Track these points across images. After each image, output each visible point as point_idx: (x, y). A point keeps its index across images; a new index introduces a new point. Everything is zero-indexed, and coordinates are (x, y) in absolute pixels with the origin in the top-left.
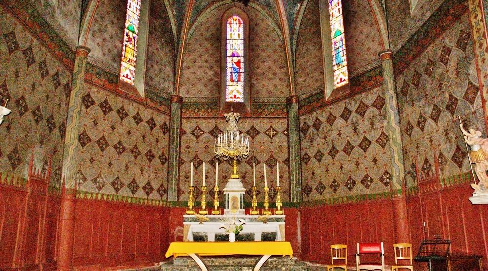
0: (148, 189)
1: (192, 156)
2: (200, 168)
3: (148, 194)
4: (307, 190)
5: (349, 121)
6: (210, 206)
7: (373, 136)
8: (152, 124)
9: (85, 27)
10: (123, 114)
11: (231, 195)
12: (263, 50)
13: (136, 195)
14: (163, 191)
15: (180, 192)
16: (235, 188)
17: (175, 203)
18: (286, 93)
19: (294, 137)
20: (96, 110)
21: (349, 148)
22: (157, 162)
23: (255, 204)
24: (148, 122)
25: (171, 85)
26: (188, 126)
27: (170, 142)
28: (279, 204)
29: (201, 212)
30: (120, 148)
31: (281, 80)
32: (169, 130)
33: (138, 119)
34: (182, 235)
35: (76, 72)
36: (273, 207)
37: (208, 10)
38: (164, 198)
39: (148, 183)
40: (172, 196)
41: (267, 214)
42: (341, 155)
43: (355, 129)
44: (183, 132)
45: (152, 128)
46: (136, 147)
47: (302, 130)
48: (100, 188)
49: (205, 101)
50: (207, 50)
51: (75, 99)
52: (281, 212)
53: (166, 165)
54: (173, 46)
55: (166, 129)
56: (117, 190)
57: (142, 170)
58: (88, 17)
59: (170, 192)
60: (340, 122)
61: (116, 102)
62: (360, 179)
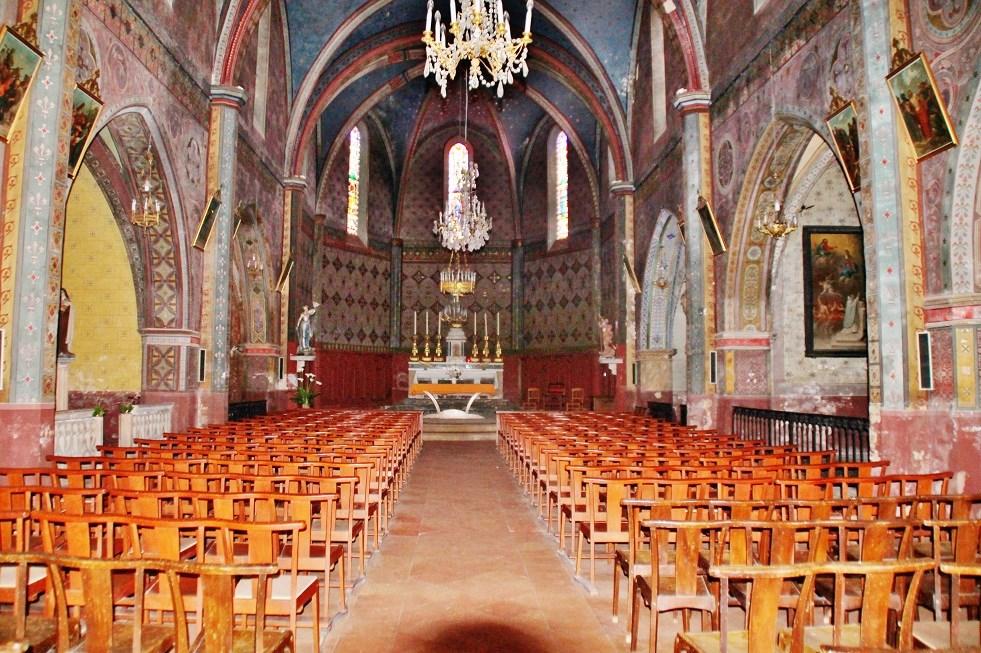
0: (374, 336)
1: (413, 301)
2: (423, 313)
3: (373, 341)
4: (527, 338)
5: (566, 276)
6: (433, 354)
7: (583, 294)
8: (375, 272)
9: (320, 195)
10: (351, 268)
11: (453, 343)
12: (488, 187)
13: (364, 343)
14: (386, 337)
15: (402, 339)
16: (456, 337)
17: (396, 349)
18: (511, 236)
19: (517, 282)
20: (331, 268)
21: (564, 302)
22: (380, 309)
23: (476, 352)
24: (372, 272)
25: (391, 228)
26: (409, 270)
27: (392, 287)
28: (499, 352)
29: (425, 359)
30: (350, 301)
31: (506, 220)
32: (390, 275)
33: (363, 270)
34: (405, 389)
35: (120, 29)
36: (492, 355)
37: (429, 139)
38: (388, 344)
39: (373, 332)
40: (394, 343)
41: (487, 361)
42: (558, 307)
43: (570, 285)
44: (404, 277)
45: (375, 277)
46: (362, 298)
47: (525, 277)
48: (336, 339)
49: (426, 244)
50: (428, 187)
51: (317, 263)
52: (500, 360)
53: (388, 312)
54: (392, 184)
55: (388, 275)
56: (349, 340)
57: (368, 319)
58: (323, 186)
59: (393, 338)
60: (558, 275)
61: (345, 257)
62: (571, 332)
